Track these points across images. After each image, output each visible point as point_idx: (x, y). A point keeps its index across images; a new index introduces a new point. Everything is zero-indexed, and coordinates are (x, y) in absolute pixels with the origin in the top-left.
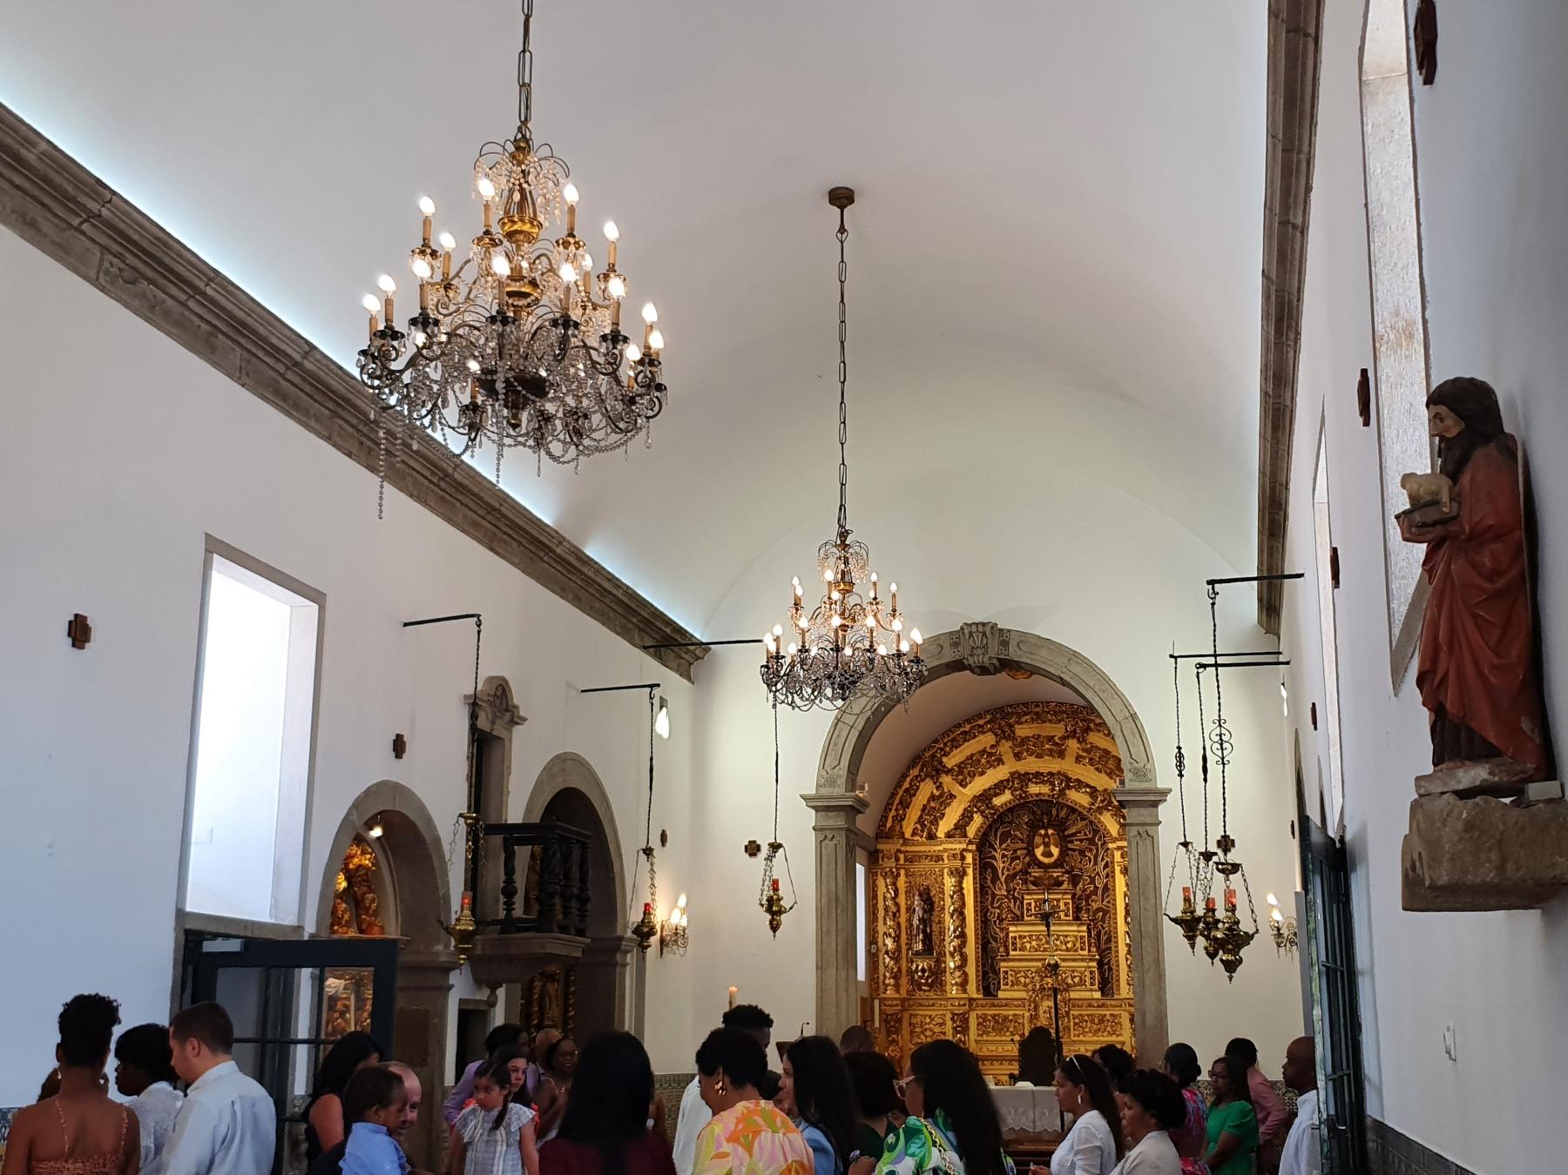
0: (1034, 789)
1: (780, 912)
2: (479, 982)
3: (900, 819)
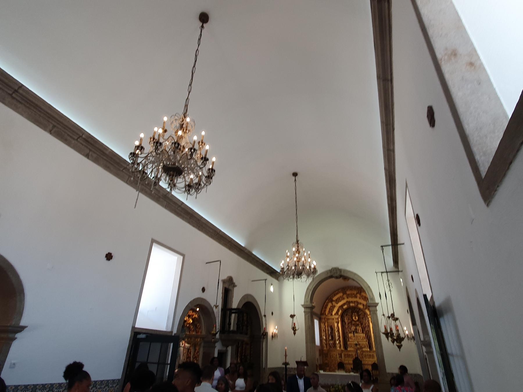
0: (351, 305)
2: (223, 345)
3: (325, 311)
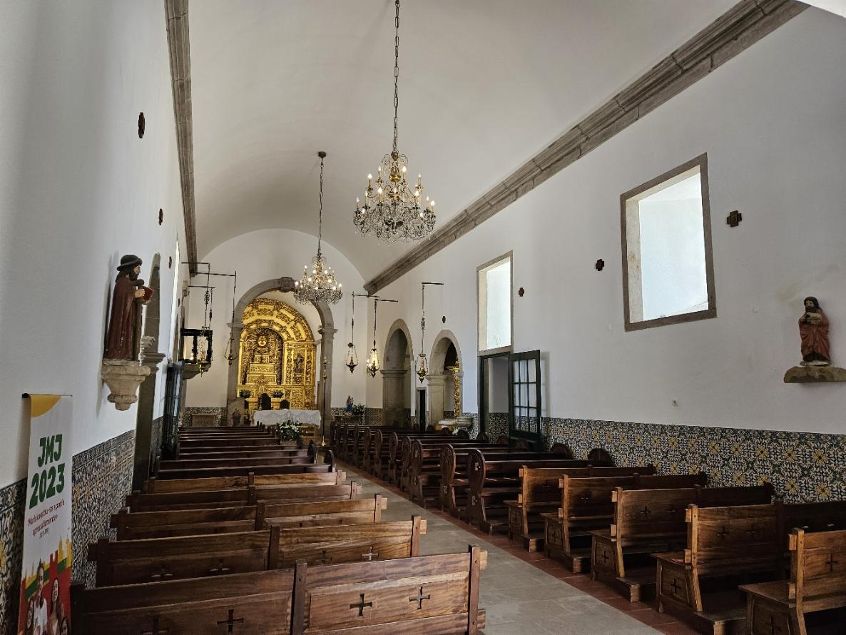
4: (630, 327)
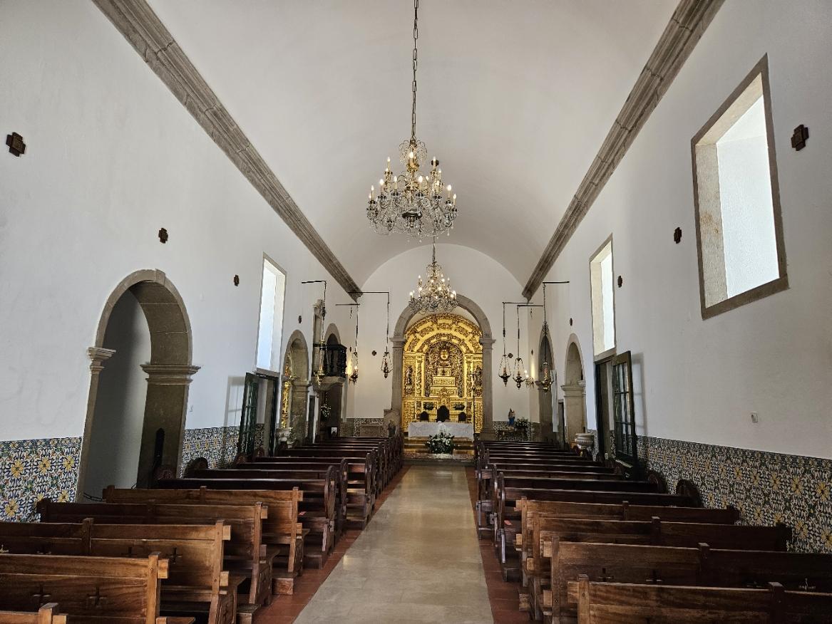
0: (442, 338)
1: (388, 372)
4: (707, 313)
